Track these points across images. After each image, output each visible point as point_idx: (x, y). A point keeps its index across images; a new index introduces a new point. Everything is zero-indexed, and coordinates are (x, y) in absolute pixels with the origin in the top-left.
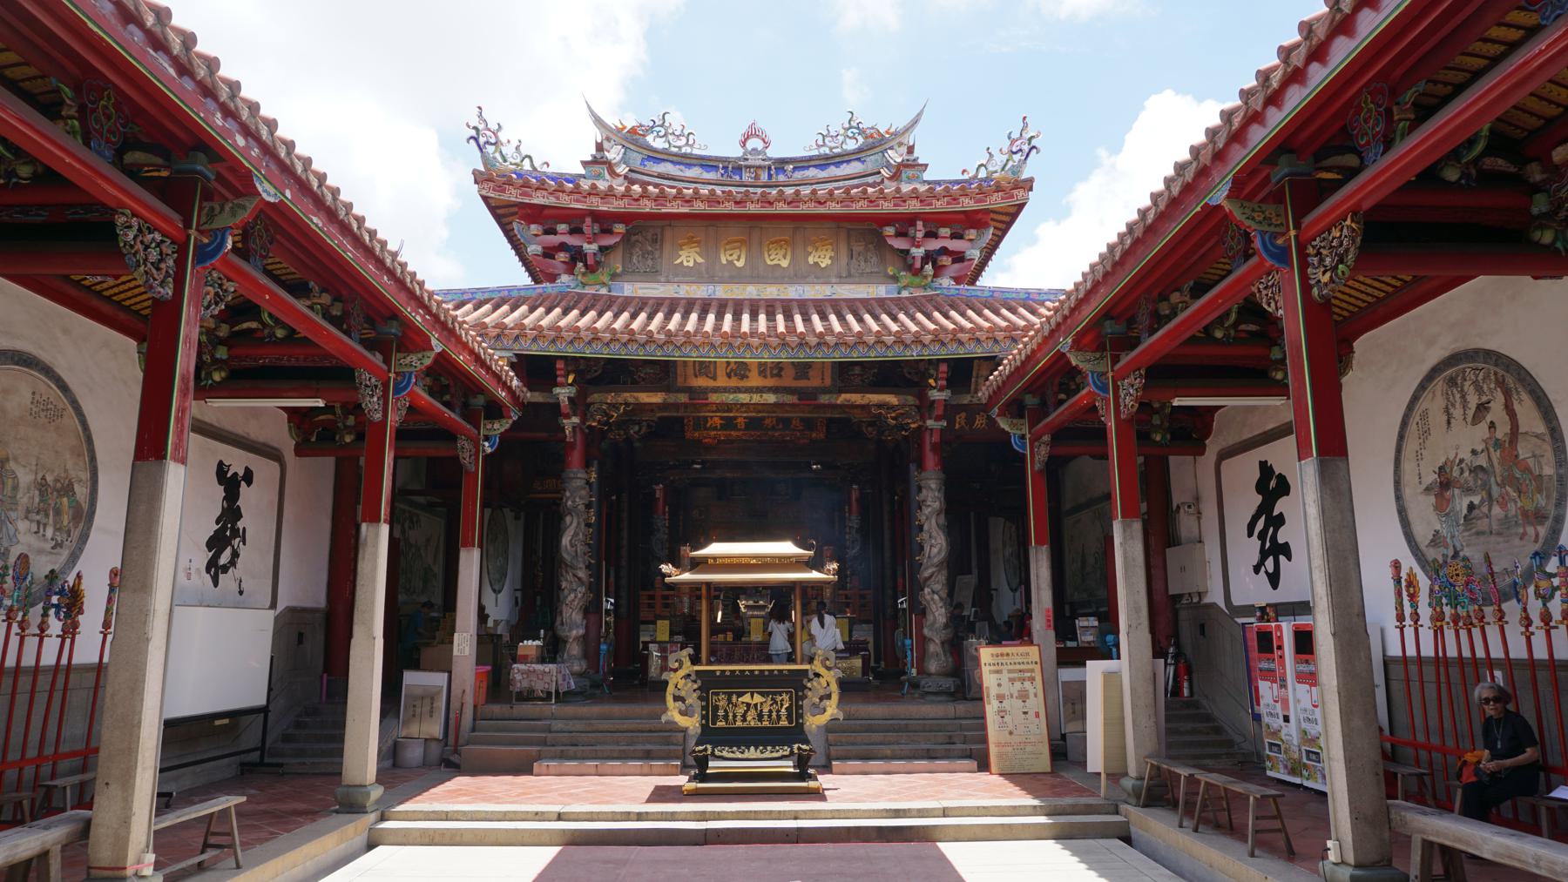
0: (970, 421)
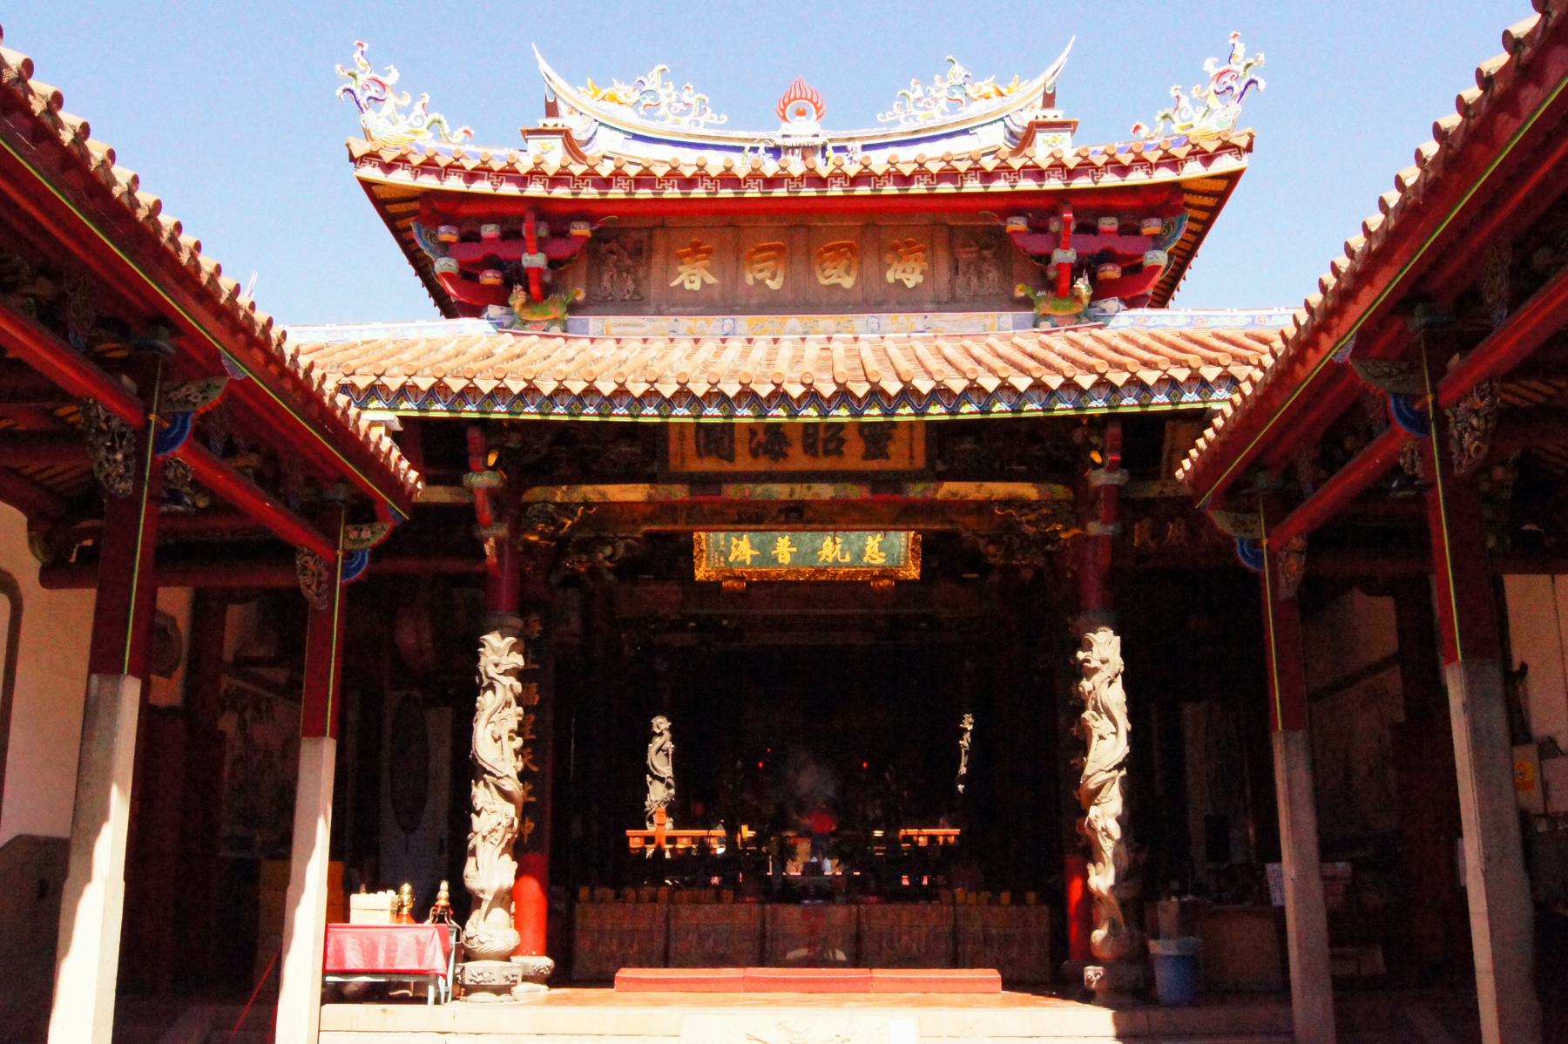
0: (1158, 533)
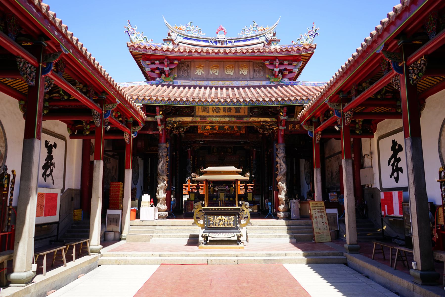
0: (294, 127)
